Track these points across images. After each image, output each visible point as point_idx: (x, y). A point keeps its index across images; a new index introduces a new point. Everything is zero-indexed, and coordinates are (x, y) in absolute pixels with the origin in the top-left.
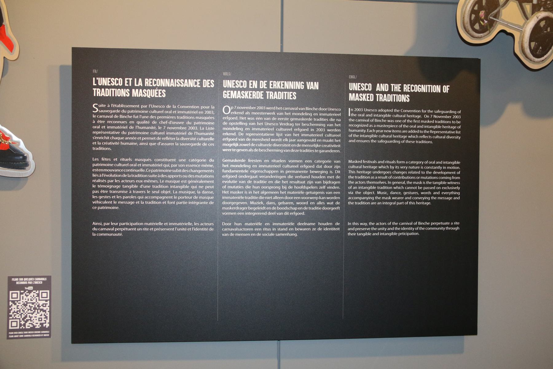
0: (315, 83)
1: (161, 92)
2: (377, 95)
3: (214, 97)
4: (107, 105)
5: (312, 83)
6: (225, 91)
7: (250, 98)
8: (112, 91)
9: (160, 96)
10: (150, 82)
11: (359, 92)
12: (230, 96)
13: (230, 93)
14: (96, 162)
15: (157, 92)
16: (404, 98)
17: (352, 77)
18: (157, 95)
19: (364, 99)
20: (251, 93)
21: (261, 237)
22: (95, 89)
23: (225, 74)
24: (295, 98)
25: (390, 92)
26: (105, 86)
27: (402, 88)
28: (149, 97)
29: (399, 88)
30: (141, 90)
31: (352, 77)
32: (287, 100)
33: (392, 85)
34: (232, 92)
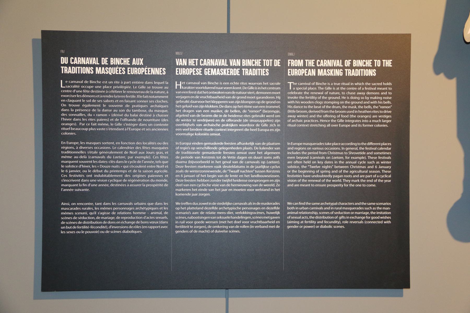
0: (237, 60)
1: (121, 69)
2: (346, 70)
4: (120, 82)
5: (234, 60)
6: (62, 58)
7: (228, 74)
8: (258, 71)
9: (120, 73)
11: (252, 67)
12: (210, 73)
13: (210, 70)
15: (118, 69)
17: (291, 54)
18: (118, 72)
19: (225, 73)
20: (229, 71)
21: (363, 224)
22: (62, 67)
23: (177, 53)
24: (267, 74)
25: (304, 67)
26: (78, 65)
27: (262, 62)
28: (110, 74)
29: (200, 72)
30: (325, 70)
32: (261, 76)
33: (384, 61)
34: (212, 69)
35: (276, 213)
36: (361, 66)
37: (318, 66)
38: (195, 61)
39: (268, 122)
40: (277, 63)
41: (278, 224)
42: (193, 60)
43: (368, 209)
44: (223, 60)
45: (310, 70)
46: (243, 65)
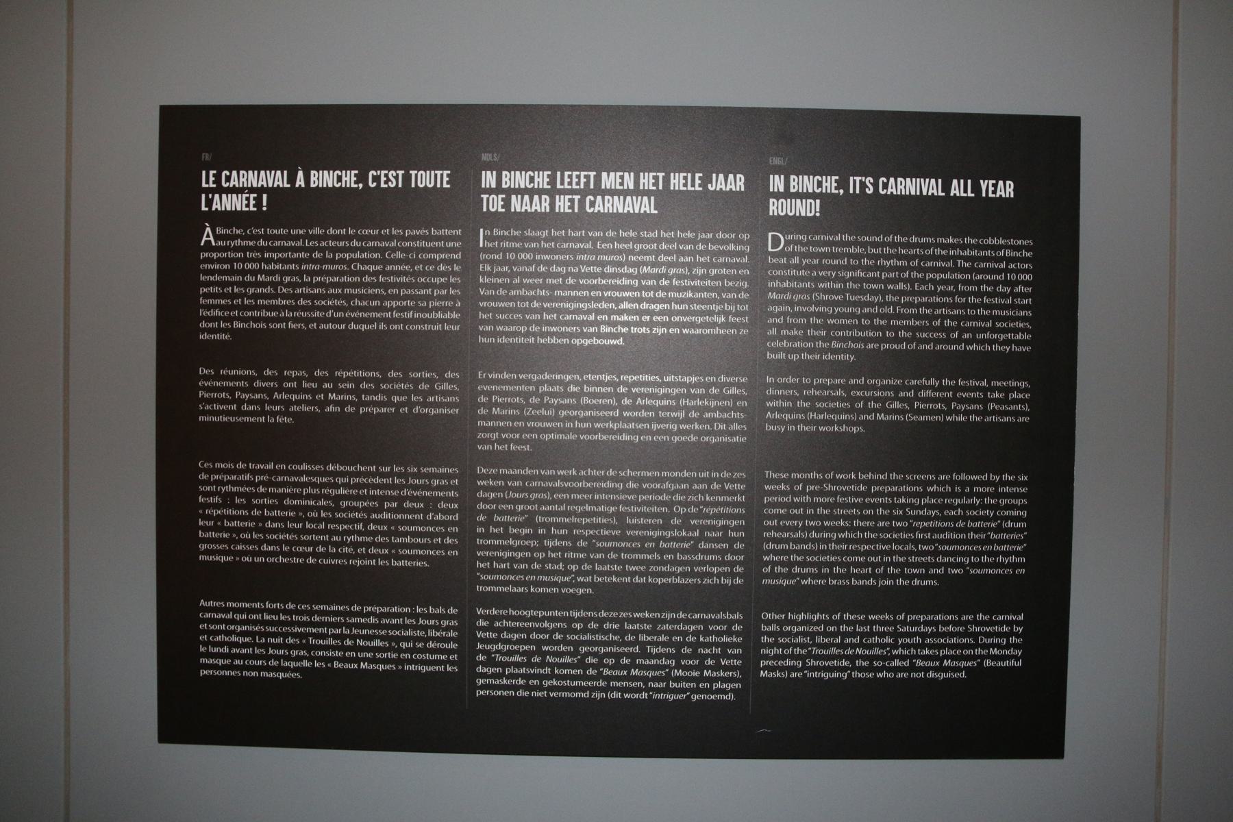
3: (459, 205)
10: (682, 181)
14: (207, 378)
15: (248, 199)
16: (646, 206)
18: (248, 206)
22: (485, 197)
23: (485, 157)
26: (239, 189)
29: (547, 180)
31: (776, 161)
33: (413, 173)
35: (771, 546)
36: (522, 186)
37: (225, 185)
38: (656, 178)
39: (718, 321)
40: (736, 183)
41: (740, 575)
42: (652, 174)
43: (953, 513)
44: (933, 181)
45: (536, 198)
46: (792, 190)
